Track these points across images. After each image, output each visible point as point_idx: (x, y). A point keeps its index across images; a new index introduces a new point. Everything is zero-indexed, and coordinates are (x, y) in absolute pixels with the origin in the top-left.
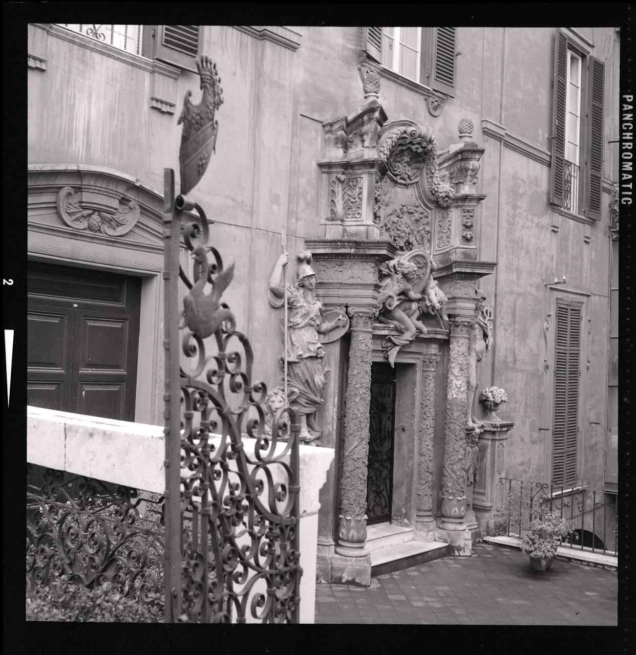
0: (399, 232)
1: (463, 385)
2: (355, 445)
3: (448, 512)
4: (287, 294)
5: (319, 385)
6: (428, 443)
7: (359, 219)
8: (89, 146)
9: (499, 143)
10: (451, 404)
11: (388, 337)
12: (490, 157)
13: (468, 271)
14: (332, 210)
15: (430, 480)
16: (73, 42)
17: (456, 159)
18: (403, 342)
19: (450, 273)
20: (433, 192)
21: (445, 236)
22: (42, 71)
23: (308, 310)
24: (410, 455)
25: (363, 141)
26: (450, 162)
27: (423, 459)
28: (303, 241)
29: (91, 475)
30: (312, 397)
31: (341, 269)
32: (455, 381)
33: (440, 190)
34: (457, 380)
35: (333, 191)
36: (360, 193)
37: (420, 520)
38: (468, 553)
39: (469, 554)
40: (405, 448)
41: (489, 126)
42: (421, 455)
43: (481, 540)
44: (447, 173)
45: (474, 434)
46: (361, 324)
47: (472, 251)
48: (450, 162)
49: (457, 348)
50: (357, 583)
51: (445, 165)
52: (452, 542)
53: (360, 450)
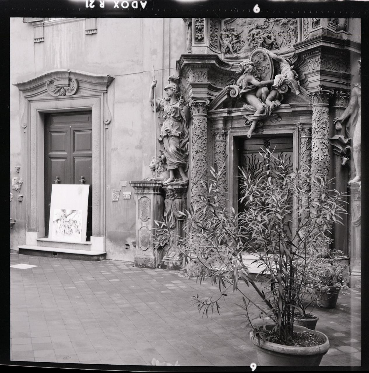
8: (61, 62)
13: (303, 50)
16: (53, 25)
22: (43, 42)
29: (18, 191)
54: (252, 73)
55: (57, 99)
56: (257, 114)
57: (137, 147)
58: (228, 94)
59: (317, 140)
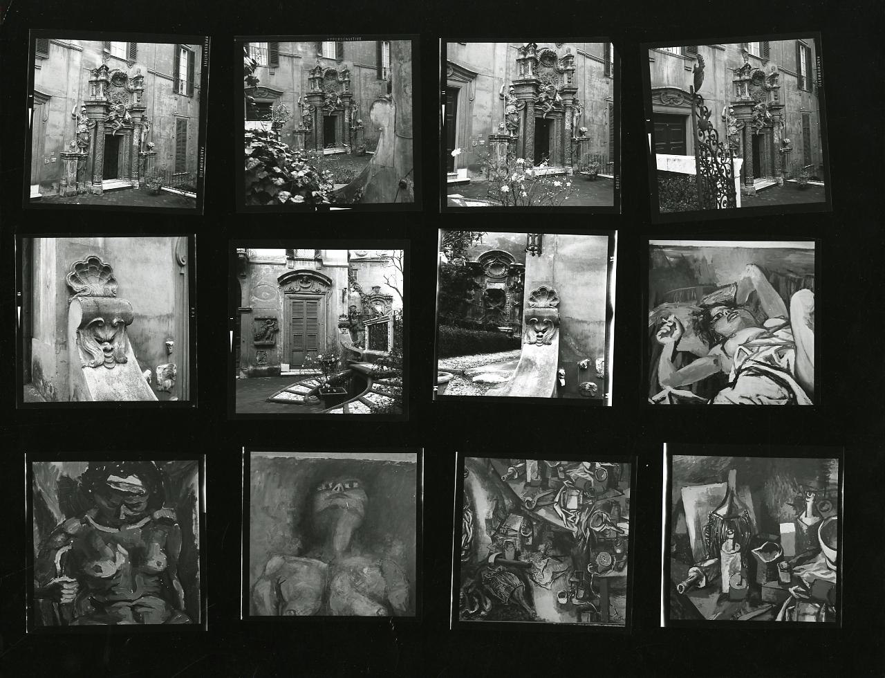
4: (77, 115)
6: (559, 143)
20: (558, 69)
55: (666, 106)
56: (549, 110)
57: (488, 116)
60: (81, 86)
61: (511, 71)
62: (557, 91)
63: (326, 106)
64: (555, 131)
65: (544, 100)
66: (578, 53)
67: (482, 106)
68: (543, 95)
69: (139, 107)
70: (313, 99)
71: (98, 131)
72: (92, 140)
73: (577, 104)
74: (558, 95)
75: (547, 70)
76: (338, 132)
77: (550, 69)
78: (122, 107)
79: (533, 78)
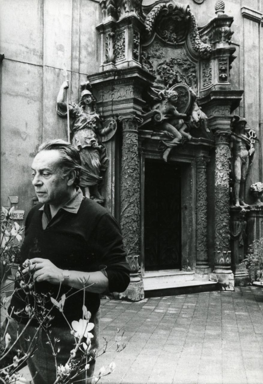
0: (168, 75)
1: (224, 175)
2: (126, 207)
3: (218, 261)
4: (69, 108)
5: (95, 166)
6: (202, 216)
7: (124, 59)
9: (257, 24)
10: (217, 189)
11: (160, 141)
12: (250, 32)
14: (106, 56)
15: (205, 240)
17: (212, 26)
18: (172, 145)
19: (209, 100)
20: (197, 50)
21: (207, 79)
23: (85, 118)
24: (191, 224)
25: (125, 9)
26: (209, 30)
27: (199, 227)
28: (86, 76)
30: (92, 174)
31: (113, 93)
32: (219, 174)
33: (200, 47)
34: (220, 172)
35: (107, 44)
36: (124, 42)
37: (199, 267)
38: (232, 289)
39: (233, 289)
40: (187, 219)
41: (247, 11)
42: (197, 224)
43: (251, 284)
44: (207, 37)
45: (241, 212)
46: (127, 126)
47: (227, 87)
48: (209, 30)
49: (219, 151)
50: (129, 299)
51: (206, 32)
52: (219, 281)
53: (129, 210)
54: (176, 104)
56: (176, 141)
58: (153, 118)
59: (225, 171)
60: (76, 39)
61: (84, 53)
62: (193, 98)
63: (157, 126)
64: (193, 189)
65: (163, 117)
66: (245, 16)
67: (16, 133)
68: (162, 109)
69: (223, 92)
70: (107, 98)
71: (125, 146)
72: (111, 170)
73: (246, 132)
74: (196, 107)
75: (172, 54)
76: (194, 219)
77: (179, 51)
78: (182, 92)
79: (134, 64)
